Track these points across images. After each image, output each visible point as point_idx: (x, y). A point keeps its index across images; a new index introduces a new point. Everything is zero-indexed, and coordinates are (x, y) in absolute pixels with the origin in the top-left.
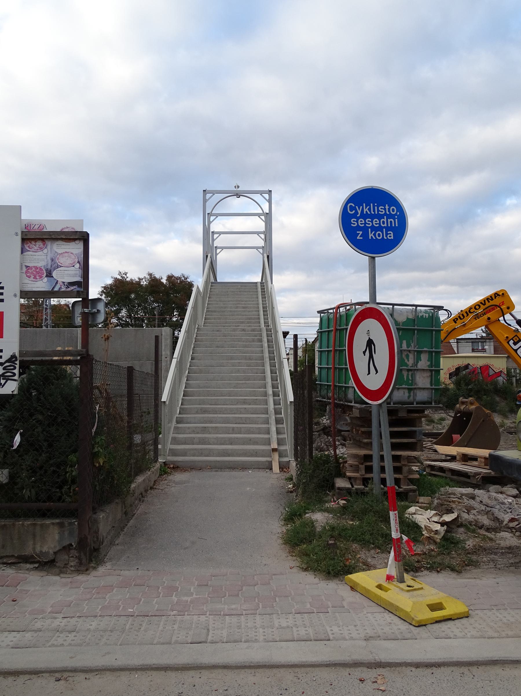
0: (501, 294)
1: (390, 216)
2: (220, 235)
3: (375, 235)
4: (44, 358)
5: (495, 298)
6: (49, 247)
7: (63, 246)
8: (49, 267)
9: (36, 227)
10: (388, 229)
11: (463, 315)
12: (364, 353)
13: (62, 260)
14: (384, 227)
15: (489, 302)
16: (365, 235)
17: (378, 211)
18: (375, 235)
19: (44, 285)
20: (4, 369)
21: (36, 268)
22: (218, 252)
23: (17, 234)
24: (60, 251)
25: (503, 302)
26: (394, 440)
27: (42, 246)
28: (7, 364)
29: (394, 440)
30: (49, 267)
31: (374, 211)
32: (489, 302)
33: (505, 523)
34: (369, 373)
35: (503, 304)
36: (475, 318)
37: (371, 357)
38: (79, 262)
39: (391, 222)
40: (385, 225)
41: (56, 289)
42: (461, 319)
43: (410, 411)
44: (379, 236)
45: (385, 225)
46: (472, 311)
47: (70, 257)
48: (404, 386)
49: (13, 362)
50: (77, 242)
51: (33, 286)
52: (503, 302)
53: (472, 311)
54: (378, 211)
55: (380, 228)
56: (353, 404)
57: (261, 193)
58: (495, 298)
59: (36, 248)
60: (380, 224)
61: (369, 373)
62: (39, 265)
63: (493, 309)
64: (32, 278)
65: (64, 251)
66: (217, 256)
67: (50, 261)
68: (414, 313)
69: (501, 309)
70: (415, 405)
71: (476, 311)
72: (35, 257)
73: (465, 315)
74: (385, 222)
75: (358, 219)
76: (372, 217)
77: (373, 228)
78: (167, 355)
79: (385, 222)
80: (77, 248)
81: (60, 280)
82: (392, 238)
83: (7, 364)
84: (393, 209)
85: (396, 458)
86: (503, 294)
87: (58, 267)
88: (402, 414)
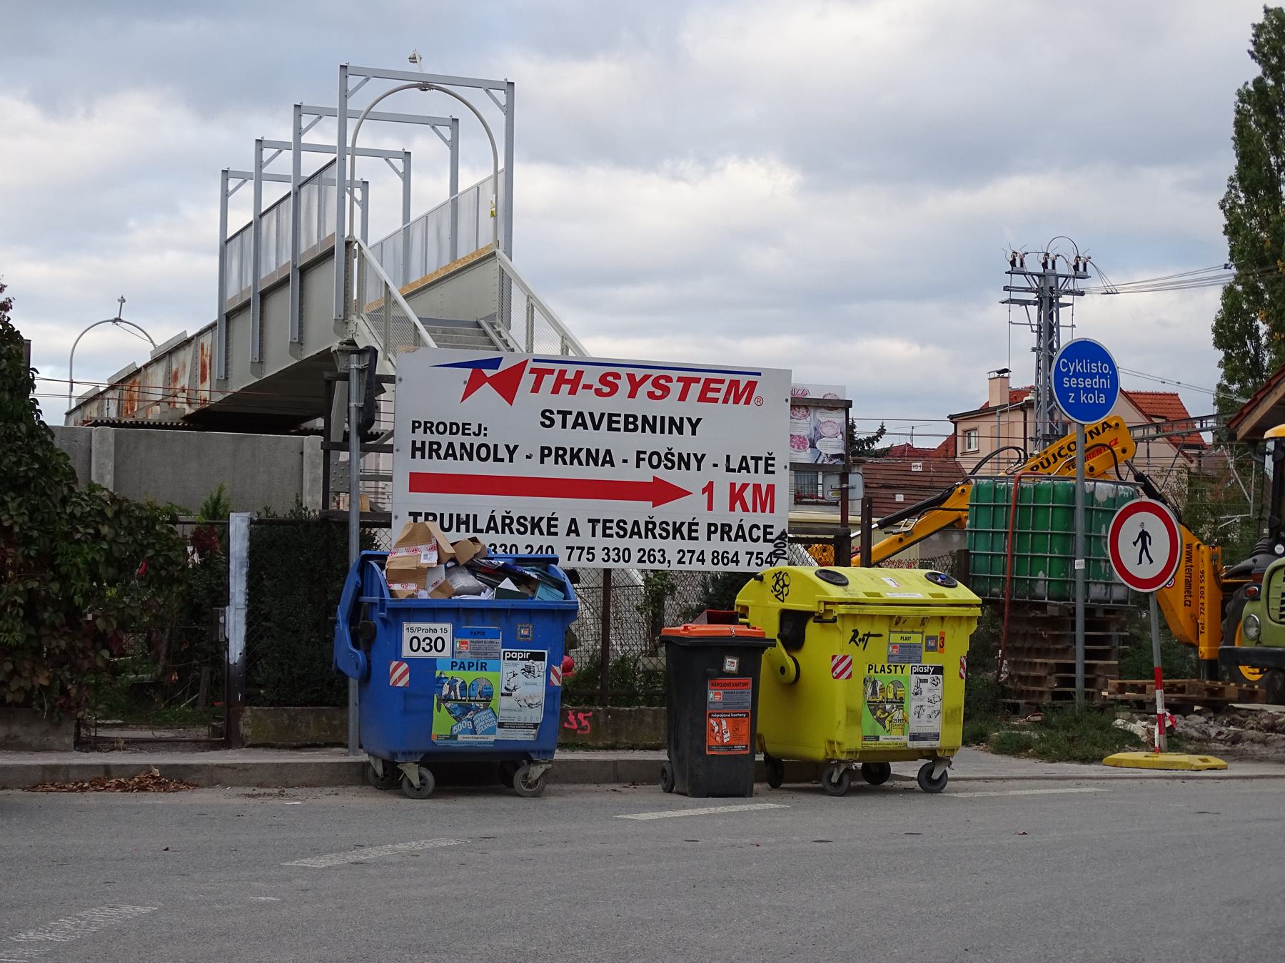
0: (1113, 424)
1: (1102, 376)
2: (281, 151)
3: (1086, 398)
4: (810, 536)
5: (1104, 431)
6: (812, 415)
7: (826, 415)
8: (812, 437)
9: (800, 392)
10: (1100, 391)
11: (1047, 460)
12: (1135, 544)
13: (826, 430)
14: (1096, 389)
15: (1092, 438)
16: (1077, 398)
17: (1091, 369)
18: (1086, 398)
19: (808, 456)
20: (775, 546)
21: (800, 437)
22: (230, 188)
23: (787, 400)
24: (823, 420)
25: (1116, 439)
26: (1087, 647)
27: (805, 413)
28: (778, 541)
29: (1087, 647)
30: (812, 437)
31: (1087, 369)
32: (1092, 438)
33: (1213, 736)
34: (1140, 562)
35: (1115, 444)
36: (1068, 467)
37: (1144, 547)
38: (841, 433)
39: (1103, 382)
40: (1098, 386)
41: (819, 462)
42: (1044, 467)
43: (1107, 612)
44: (1090, 399)
45: (1098, 386)
46: (1063, 453)
47: (832, 426)
48: (1101, 580)
49: (783, 539)
50: (839, 410)
51: (797, 456)
52: (1116, 439)
53: (1063, 453)
54: (1091, 369)
55: (1092, 390)
56: (1046, 600)
57: (488, 86)
58: (1104, 431)
59: (799, 415)
60: (1092, 385)
61: (1140, 562)
62: (802, 434)
63: (1099, 452)
64: (796, 449)
65: (827, 419)
66: (229, 199)
67: (813, 430)
68: (1114, 491)
69: (1113, 451)
70: (1111, 604)
71: (1070, 453)
72: (799, 425)
73: (1052, 460)
74: (1097, 383)
75: (1070, 377)
76: (1085, 376)
77: (1086, 391)
78: (317, 503)
79: (1097, 383)
80: (838, 418)
81: (824, 452)
82: (1104, 402)
83: (778, 541)
84: (1106, 367)
85: (1088, 669)
86: (1117, 425)
87: (821, 437)
88: (1100, 614)
